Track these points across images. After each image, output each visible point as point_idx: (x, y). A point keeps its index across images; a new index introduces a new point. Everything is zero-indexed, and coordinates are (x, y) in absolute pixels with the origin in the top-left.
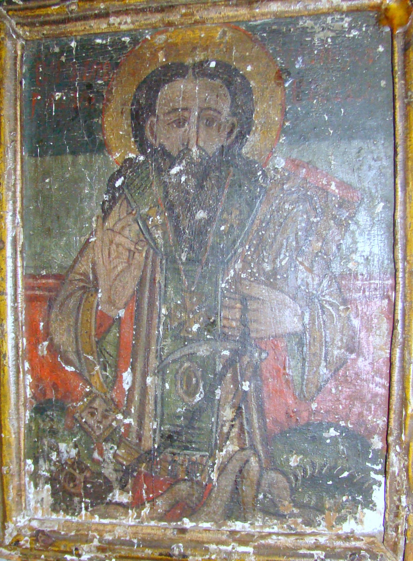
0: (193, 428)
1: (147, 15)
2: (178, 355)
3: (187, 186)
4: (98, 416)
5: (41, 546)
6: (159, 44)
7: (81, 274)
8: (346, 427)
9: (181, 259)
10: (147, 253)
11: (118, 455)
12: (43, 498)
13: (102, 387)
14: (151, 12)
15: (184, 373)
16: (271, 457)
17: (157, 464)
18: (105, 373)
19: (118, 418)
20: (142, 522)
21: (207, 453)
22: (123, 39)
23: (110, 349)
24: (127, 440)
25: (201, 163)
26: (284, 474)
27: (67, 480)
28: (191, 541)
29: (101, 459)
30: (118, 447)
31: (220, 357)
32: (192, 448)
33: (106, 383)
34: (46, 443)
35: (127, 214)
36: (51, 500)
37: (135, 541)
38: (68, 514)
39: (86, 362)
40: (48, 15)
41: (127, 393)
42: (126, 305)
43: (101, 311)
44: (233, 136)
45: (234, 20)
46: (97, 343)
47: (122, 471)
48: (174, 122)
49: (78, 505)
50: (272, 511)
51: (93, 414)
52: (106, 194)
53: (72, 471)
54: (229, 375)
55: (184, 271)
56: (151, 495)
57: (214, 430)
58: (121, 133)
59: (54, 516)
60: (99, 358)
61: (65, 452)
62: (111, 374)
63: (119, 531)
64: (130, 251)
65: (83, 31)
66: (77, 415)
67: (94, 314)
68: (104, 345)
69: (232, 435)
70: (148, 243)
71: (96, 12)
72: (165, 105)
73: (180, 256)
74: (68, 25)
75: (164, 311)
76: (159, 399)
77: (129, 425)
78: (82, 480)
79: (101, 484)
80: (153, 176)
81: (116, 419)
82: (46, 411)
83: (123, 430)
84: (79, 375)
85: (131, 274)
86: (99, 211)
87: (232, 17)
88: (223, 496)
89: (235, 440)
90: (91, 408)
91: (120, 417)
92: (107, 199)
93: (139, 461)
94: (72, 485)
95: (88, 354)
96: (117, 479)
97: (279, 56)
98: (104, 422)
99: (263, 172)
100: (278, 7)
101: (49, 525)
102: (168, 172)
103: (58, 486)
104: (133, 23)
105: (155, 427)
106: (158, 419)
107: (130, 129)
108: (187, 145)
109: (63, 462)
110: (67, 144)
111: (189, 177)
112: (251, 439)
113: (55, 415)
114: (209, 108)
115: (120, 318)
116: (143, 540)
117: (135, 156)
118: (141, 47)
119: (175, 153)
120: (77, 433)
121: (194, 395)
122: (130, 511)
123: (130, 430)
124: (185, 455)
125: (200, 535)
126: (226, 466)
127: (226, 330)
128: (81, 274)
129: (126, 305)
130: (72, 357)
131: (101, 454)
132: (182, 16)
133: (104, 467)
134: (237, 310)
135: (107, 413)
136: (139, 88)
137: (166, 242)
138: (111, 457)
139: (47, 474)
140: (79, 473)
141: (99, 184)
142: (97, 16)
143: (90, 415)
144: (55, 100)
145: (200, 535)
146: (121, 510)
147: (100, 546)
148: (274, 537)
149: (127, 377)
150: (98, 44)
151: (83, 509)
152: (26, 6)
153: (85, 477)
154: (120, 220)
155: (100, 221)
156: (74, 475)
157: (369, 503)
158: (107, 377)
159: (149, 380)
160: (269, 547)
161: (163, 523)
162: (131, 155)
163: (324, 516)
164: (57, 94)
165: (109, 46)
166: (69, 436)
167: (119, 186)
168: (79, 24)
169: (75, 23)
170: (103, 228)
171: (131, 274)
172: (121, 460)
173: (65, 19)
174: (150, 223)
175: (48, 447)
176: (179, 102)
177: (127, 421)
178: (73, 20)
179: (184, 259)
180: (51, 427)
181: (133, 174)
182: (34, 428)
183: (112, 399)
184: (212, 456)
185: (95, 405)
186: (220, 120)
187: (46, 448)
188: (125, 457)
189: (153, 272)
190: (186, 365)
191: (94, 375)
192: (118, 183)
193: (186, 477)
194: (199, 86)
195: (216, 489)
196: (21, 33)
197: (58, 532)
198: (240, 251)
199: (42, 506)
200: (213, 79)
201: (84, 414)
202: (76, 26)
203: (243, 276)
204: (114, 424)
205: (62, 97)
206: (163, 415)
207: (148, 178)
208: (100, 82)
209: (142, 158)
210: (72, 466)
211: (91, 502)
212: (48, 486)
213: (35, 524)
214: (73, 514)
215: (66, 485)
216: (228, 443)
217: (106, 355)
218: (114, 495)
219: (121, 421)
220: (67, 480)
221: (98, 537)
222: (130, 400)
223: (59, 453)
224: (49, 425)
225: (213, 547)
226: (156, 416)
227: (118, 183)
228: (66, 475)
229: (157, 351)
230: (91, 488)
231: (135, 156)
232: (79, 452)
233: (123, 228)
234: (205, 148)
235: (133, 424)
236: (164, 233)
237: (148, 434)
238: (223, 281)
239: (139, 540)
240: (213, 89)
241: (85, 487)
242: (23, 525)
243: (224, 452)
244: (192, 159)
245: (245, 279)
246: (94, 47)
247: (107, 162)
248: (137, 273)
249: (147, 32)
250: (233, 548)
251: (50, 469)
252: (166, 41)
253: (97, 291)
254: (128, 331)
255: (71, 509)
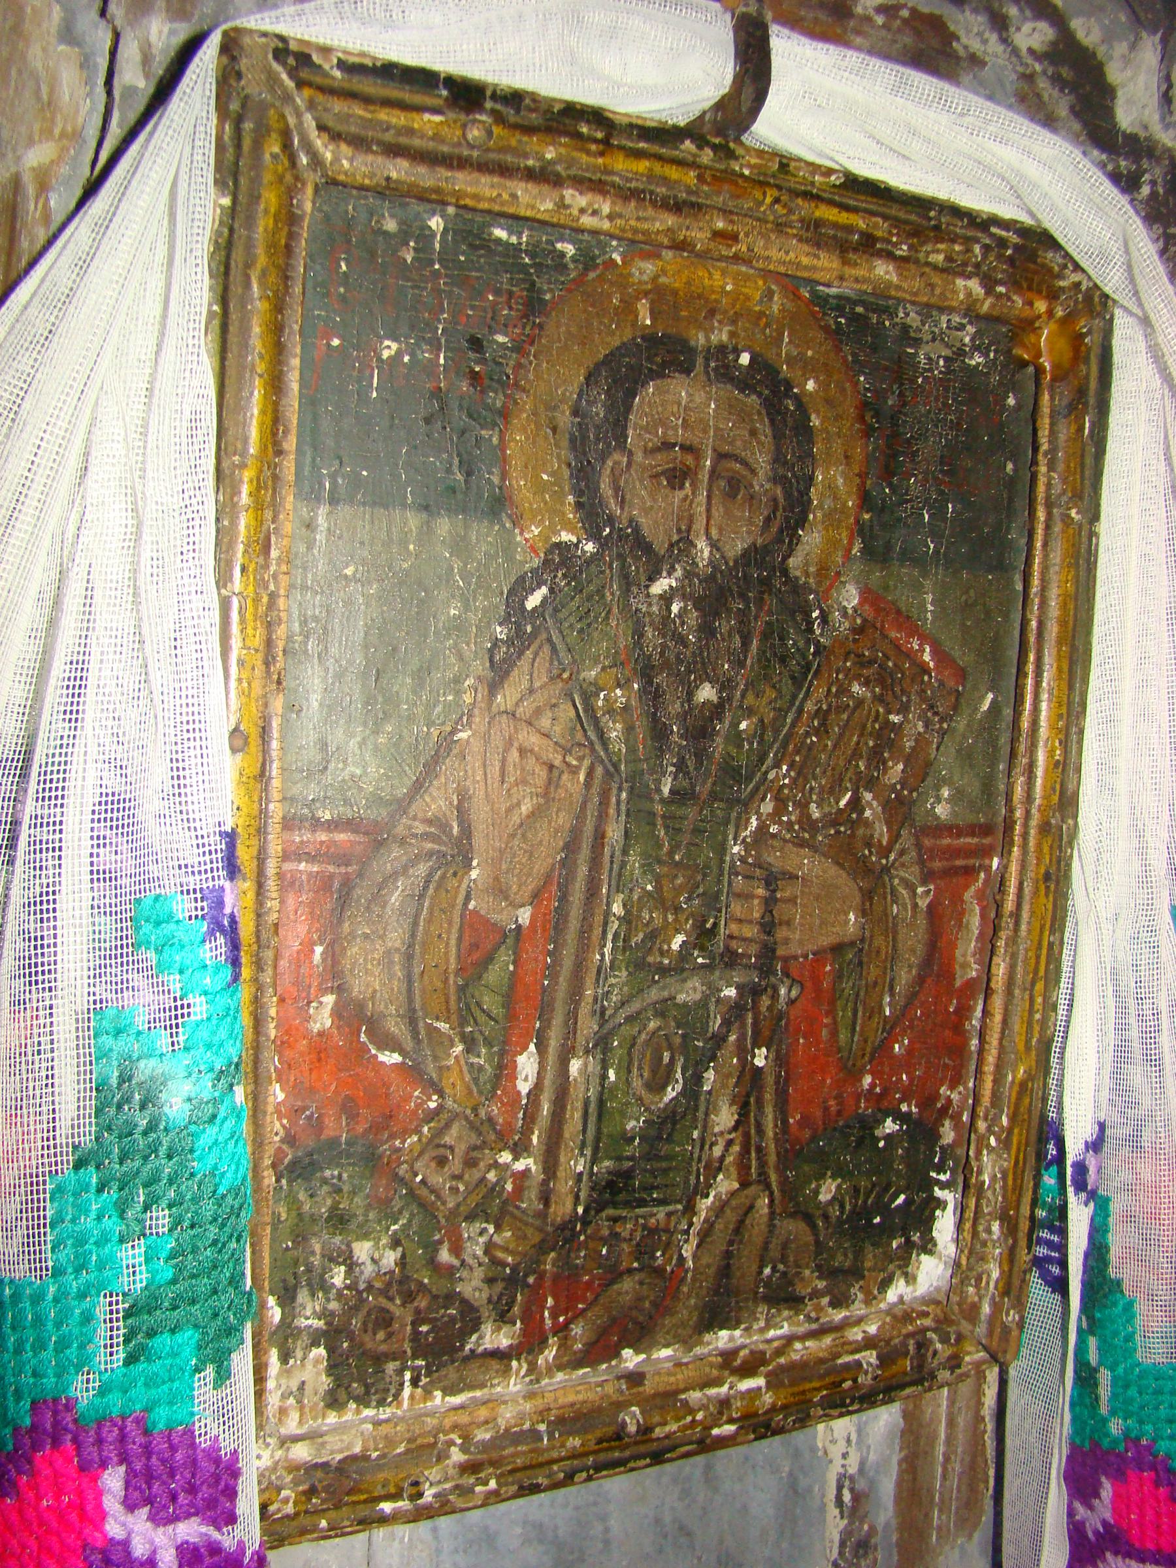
0: (658, 1158)
1: (645, 209)
2: (635, 1006)
3: (683, 624)
4: (455, 1165)
5: (324, 1501)
6: (640, 282)
7: (430, 822)
8: (910, 1113)
9: (659, 790)
10: (590, 774)
11: (496, 1245)
12: (303, 1383)
13: (470, 1092)
14: (653, 203)
15: (647, 1042)
16: (790, 1191)
17: (579, 1250)
18: (476, 1060)
19: (501, 1161)
20: (538, 1381)
21: (679, 1207)
22: (559, 246)
23: (490, 1002)
24: (518, 1208)
25: (712, 577)
26: (809, 1219)
27: (370, 1326)
28: (655, 1395)
29: (456, 1262)
30: (498, 1228)
31: (718, 1001)
32: (654, 1200)
33: (477, 1084)
34: (317, 1248)
35: (552, 679)
36: (325, 1382)
37: (542, 1427)
38: (367, 1406)
39: (430, 1038)
40: (410, 132)
41: (524, 1101)
42: (536, 897)
43: (475, 912)
44: (774, 529)
45: (806, 274)
46: (462, 989)
47: (503, 1280)
48: (663, 473)
49: (396, 1378)
50: (784, 1297)
51: (442, 1162)
52: (500, 624)
53: (383, 1302)
54: (733, 1038)
55: (664, 817)
56: (561, 1319)
57: (696, 1155)
58: (545, 477)
59: (332, 1418)
60: (463, 1022)
61: (369, 1262)
62: (489, 1060)
63: (506, 1415)
64: (551, 767)
65: (492, 200)
66: (403, 1170)
67: (457, 919)
68: (477, 993)
69: (730, 1159)
70: (593, 750)
71: (530, 162)
72: (646, 429)
73: (658, 782)
74: (460, 175)
75: (617, 908)
76: (593, 1108)
77: (526, 1173)
78: (409, 1319)
79: (453, 1319)
80: (612, 594)
81: (496, 1165)
82: (322, 1169)
83: (509, 1187)
84: (412, 1072)
85: (550, 822)
86: (480, 666)
87: (806, 268)
88: (701, 1287)
89: (732, 1169)
90: (438, 1146)
91: (505, 1157)
92: (504, 636)
93: (542, 1248)
94: (381, 1335)
95: (437, 1019)
96: (490, 1301)
97: (864, 374)
98: (466, 1177)
99: (822, 611)
100: (887, 273)
101: (339, 1446)
102: (647, 587)
103: (345, 1345)
104: (610, 217)
105: (580, 1168)
106: (588, 1152)
107: (566, 473)
108: (689, 530)
109: (362, 1286)
110: (409, 482)
111: (686, 606)
112: (762, 1164)
113: (345, 1176)
114: (736, 458)
115: (519, 927)
116: (561, 1421)
117: (575, 540)
118: (599, 277)
119: (660, 546)
120: (400, 1212)
121: (662, 1088)
122: (514, 1363)
123: (527, 1184)
124: (637, 1217)
125: (672, 1379)
126: (712, 1225)
127: (734, 944)
128: (430, 822)
129: (536, 897)
130: (395, 1027)
131: (456, 1250)
132: (717, 235)
133: (461, 1279)
134: (756, 902)
135: (475, 1154)
136: (591, 378)
137: (632, 750)
138: (479, 1253)
139: (319, 1324)
140: (403, 1305)
141: (486, 597)
142: (531, 175)
143: (433, 1164)
144: (380, 359)
145: (672, 1379)
146: (495, 1364)
147: (468, 1461)
148: (798, 1345)
149: (527, 1064)
150: (498, 241)
151: (407, 1384)
152: (346, 85)
153: (418, 1311)
154: (531, 691)
155: (483, 691)
156: (388, 1311)
157: (928, 1245)
158: (481, 1068)
159: (575, 1066)
160: (792, 1366)
161: (581, 1372)
162: (566, 537)
163: (861, 1283)
164: (387, 343)
165: (526, 252)
166: (379, 1222)
167: (535, 609)
168: (485, 179)
169: (476, 175)
170: (489, 709)
171: (550, 822)
172: (500, 1255)
173: (451, 158)
174: (600, 703)
175: (323, 1256)
176: (675, 428)
177: (520, 1166)
178: (471, 165)
179: (666, 790)
180: (334, 1208)
181: (569, 584)
182: (284, 1216)
183: (490, 1120)
184: (690, 1209)
185: (447, 1140)
186: (752, 486)
187: (316, 1261)
188: (512, 1246)
189: (602, 816)
190: (652, 1025)
191: (448, 1068)
192: (533, 601)
193: (635, 1265)
194: (716, 401)
195: (690, 1275)
196: (328, 156)
197: (364, 1457)
198: (771, 775)
199: (299, 1402)
200: (742, 391)
201: (418, 1165)
202: (478, 182)
203: (774, 829)
204: (492, 1176)
205: (399, 354)
206: (597, 1139)
207: (603, 596)
208: (501, 339)
209: (590, 547)
210: (385, 1293)
211: (428, 1366)
212: (321, 1351)
213: (302, 1452)
214: (381, 1403)
215: (367, 1338)
216: (721, 1176)
217: (482, 1018)
218: (481, 1337)
219: (507, 1166)
220: (370, 1326)
221: (459, 1441)
222: (530, 1118)
223: (351, 1266)
224: (329, 1202)
225: (695, 1396)
226: (583, 1146)
227: (533, 601)
228: (369, 1314)
229: (596, 1000)
230: (428, 1332)
231: (575, 540)
232: (403, 1256)
233: (538, 712)
234: (720, 544)
235: (534, 1168)
236: (629, 729)
237: (564, 1186)
238: (735, 839)
239: (550, 1423)
240: (743, 416)
241: (416, 1334)
242: (269, 1463)
243: (711, 1198)
244: (695, 564)
245: (773, 836)
246: (488, 245)
247: (508, 549)
248: (563, 820)
249: (614, 243)
250: (731, 1388)
251: (325, 1308)
252: (655, 279)
253: (468, 867)
254: (536, 954)
255: (373, 1391)
